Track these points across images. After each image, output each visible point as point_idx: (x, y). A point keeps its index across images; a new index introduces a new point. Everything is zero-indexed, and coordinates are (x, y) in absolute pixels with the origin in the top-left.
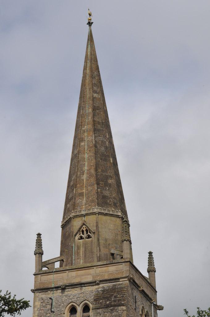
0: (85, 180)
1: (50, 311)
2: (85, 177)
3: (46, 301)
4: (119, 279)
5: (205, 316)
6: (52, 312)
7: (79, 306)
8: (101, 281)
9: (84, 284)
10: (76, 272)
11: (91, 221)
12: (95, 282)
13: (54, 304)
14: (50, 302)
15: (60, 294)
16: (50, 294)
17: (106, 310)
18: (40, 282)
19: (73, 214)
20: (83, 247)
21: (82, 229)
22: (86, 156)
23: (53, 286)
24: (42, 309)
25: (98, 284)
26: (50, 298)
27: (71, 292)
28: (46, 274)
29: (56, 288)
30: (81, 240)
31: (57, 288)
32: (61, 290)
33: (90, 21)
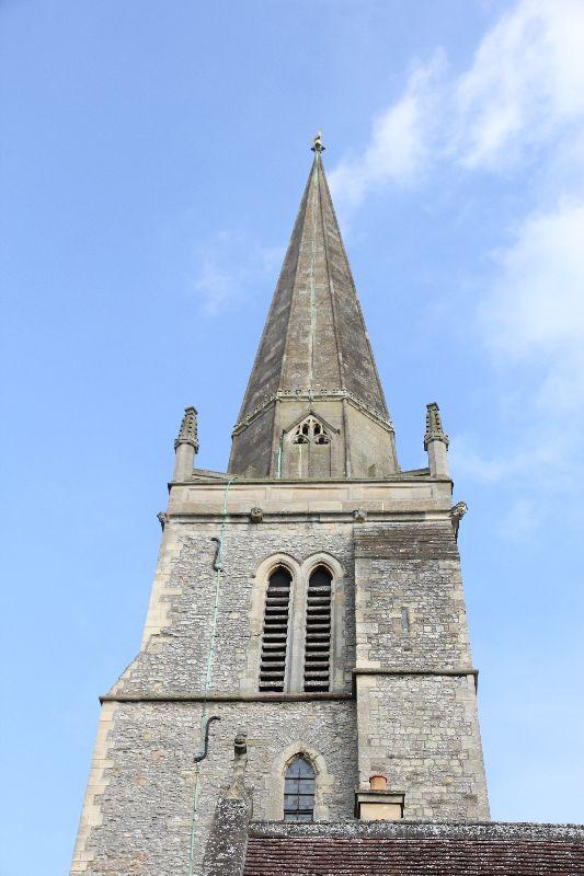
0: (310, 346)
1: (209, 568)
2: (310, 341)
3: (200, 546)
4: (422, 513)
5: (188, 874)
6: (216, 569)
7: (300, 563)
8: (369, 514)
9: (318, 514)
10: (295, 491)
11: (330, 411)
12: (352, 514)
13: (222, 552)
14: (213, 549)
15: (244, 534)
16: (213, 530)
17: (402, 565)
18: (184, 501)
19: (280, 394)
20: (304, 457)
21: (305, 421)
22: (313, 310)
23: (225, 512)
24: (185, 559)
25: (360, 520)
26: (214, 539)
27: (277, 532)
28: (189, 521)
29: (233, 516)
30: (300, 446)
31: (236, 517)
32: (246, 526)
33: (319, 141)
